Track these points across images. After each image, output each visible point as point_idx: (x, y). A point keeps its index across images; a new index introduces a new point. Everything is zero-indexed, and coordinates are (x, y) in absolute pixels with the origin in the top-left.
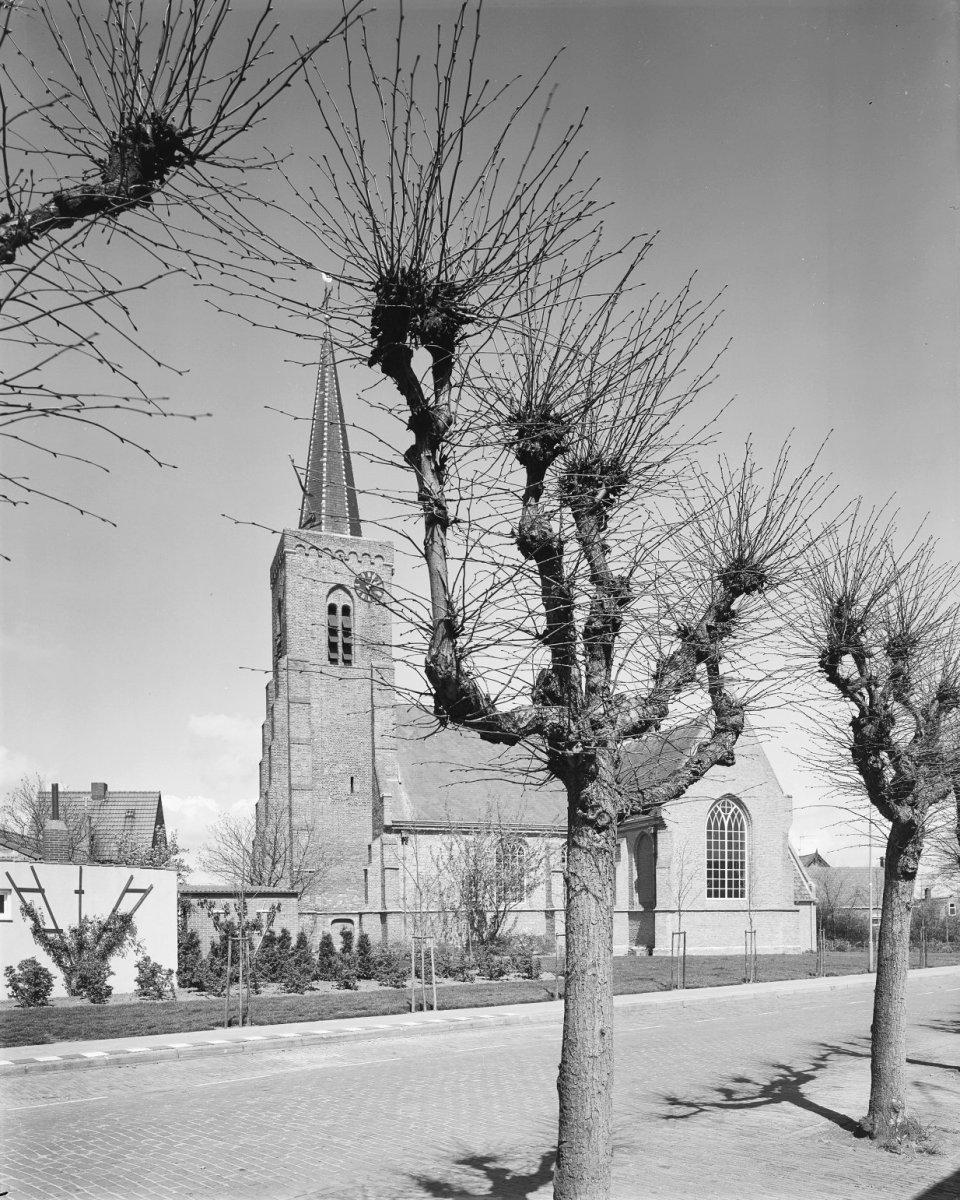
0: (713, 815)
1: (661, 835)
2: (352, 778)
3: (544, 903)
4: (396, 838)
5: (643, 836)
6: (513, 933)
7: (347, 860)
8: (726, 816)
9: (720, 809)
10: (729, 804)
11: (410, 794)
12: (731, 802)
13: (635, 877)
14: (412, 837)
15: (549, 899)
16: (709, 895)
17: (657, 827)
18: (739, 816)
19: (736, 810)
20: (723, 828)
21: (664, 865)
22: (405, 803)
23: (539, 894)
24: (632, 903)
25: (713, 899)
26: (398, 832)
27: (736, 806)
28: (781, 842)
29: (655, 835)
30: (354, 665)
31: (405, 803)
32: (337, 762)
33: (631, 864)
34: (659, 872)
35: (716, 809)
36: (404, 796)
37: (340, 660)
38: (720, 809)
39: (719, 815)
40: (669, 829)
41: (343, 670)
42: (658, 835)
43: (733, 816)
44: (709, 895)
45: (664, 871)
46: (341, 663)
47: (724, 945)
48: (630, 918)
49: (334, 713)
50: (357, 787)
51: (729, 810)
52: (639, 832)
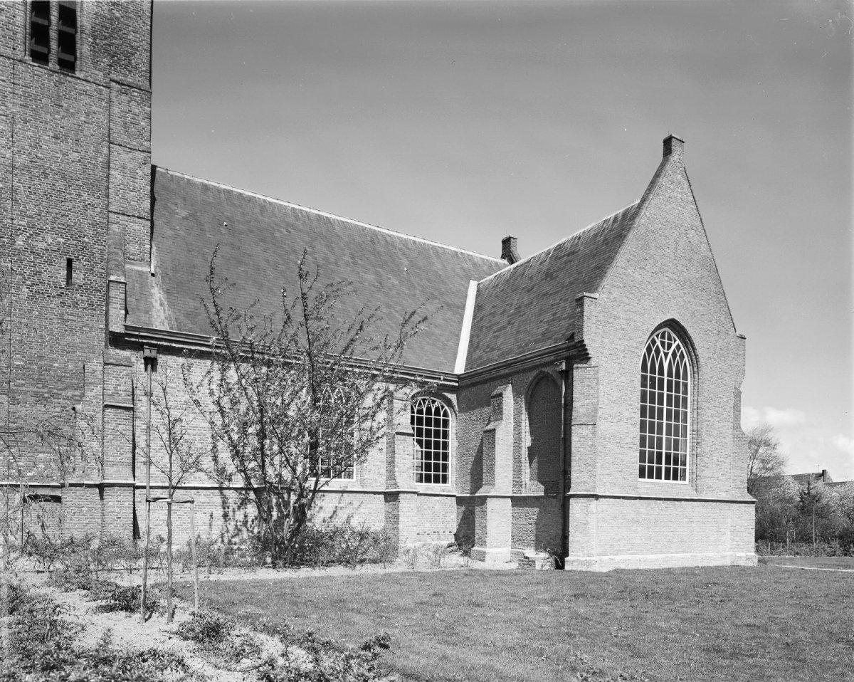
0: (649, 350)
1: (579, 373)
2: (70, 262)
3: (383, 481)
4: (136, 359)
5: (542, 379)
6: (339, 522)
7: (57, 396)
8: (666, 355)
9: (658, 343)
10: (670, 338)
11: (168, 292)
12: (673, 335)
13: (527, 441)
14: (162, 359)
15: (391, 475)
16: (642, 475)
17: (571, 361)
18: (682, 356)
19: (678, 347)
20: (661, 372)
21: (584, 420)
22: (157, 305)
23: (376, 456)
24: (517, 483)
25: (646, 480)
26: (138, 347)
27: (678, 342)
28: (732, 402)
29: (567, 375)
30: (78, 74)
31: (157, 305)
32: (42, 230)
33: (518, 425)
34: (576, 431)
35: (654, 342)
36: (157, 294)
37: (53, 58)
38: (658, 343)
39: (658, 351)
40: (593, 362)
41: (56, 77)
42: (575, 373)
43: (674, 355)
44: (642, 475)
45: (585, 431)
46: (53, 64)
47: (661, 552)
48: (386, 501)
49: (36, 146)
50: (78, 277)
51: (670, 346)
52: (534, 373)
